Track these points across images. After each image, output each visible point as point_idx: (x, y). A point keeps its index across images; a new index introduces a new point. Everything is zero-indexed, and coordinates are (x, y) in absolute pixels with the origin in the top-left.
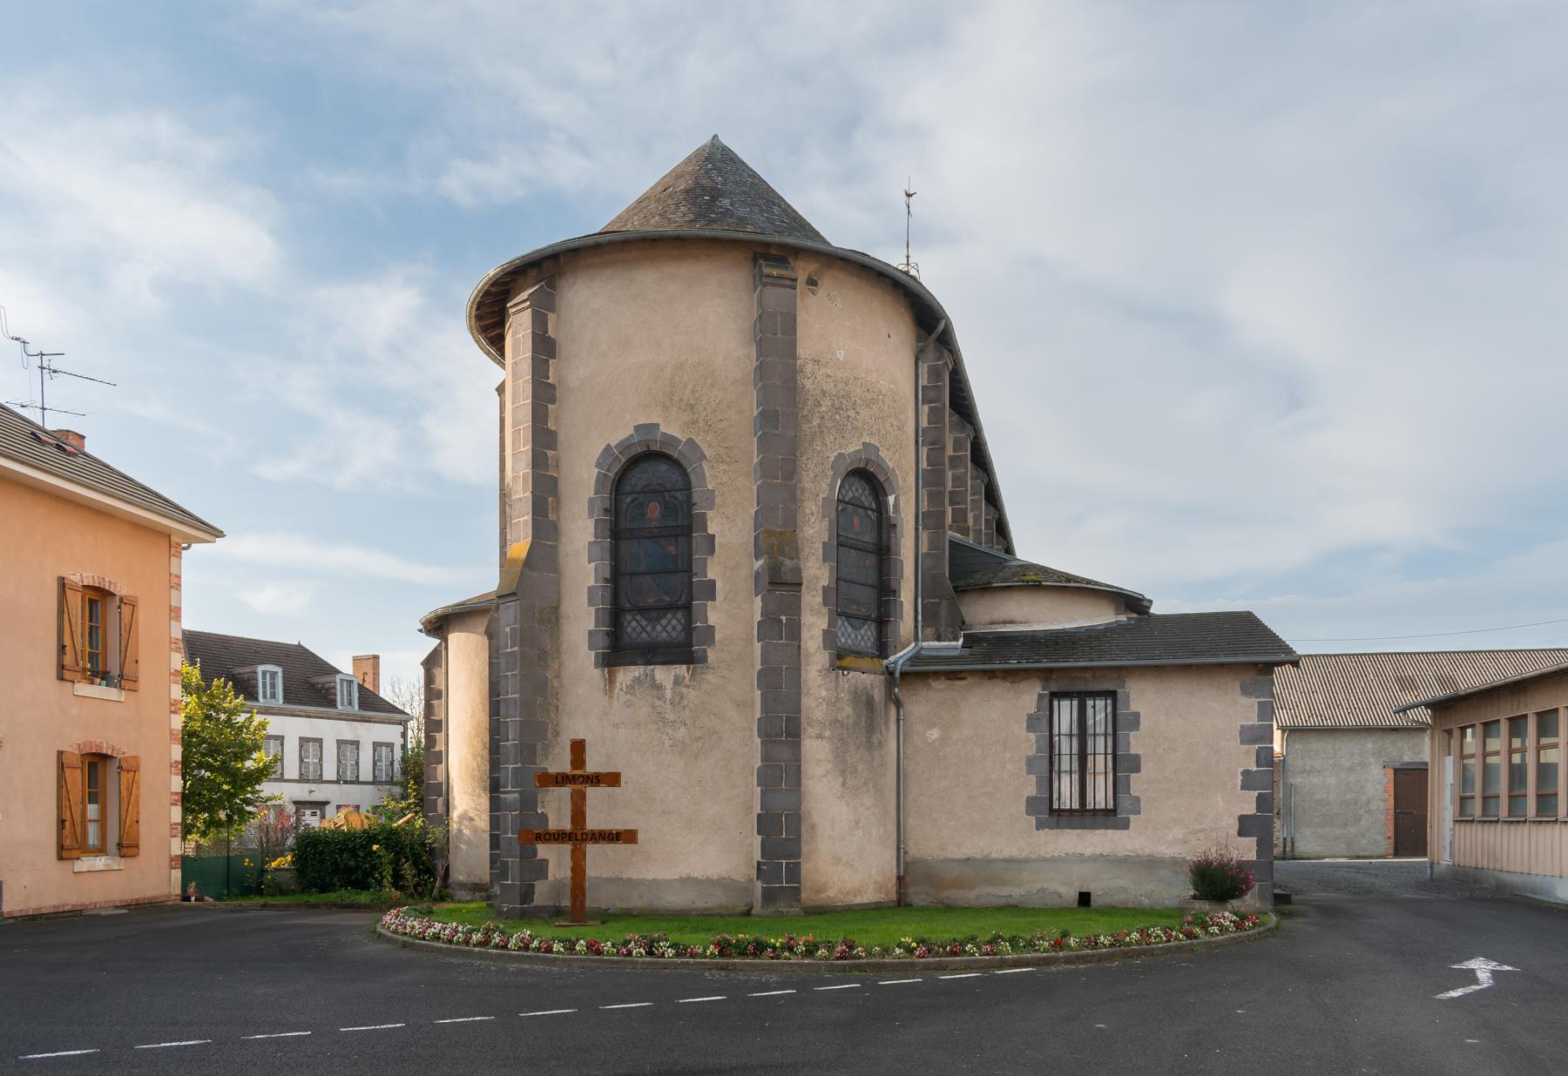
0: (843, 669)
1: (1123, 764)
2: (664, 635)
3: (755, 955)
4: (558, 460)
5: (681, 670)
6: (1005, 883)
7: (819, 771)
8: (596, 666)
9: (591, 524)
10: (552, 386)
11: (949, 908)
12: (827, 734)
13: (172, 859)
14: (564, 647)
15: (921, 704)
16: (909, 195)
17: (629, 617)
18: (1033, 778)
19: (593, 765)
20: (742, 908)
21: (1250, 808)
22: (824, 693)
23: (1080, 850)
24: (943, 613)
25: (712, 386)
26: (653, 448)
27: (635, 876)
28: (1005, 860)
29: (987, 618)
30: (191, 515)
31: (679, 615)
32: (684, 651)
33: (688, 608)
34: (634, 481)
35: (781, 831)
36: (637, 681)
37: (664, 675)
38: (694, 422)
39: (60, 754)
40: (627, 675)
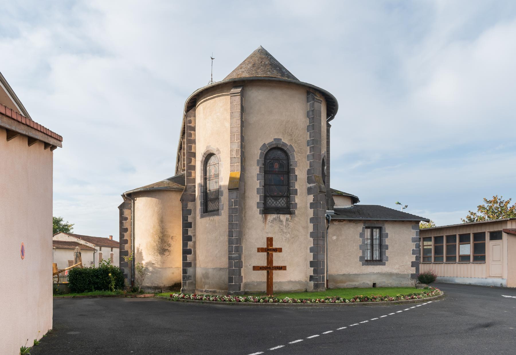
1: (382, 247)
2: (280, 205)
3: (366, 301)
5: (288, 216)
6: (354, 281)
8: (260, 214)
9: (258, 168)
11: (339, 289)
14: (247, 207)
17: (268, 199)
19: (275, 245)
20: (304, 290)
21: (414, 260)
23: (373, 271)
25: (297, 129)
26: (279, 146)
27: (278, 281)
28: (354, 275)
31: (284, 199)
32: (288, 210)
33: (288, 197)
34: (270, 156)
36: (275, 219)
37: (283, 217)
38: (292, 140)
40: (271, 217)
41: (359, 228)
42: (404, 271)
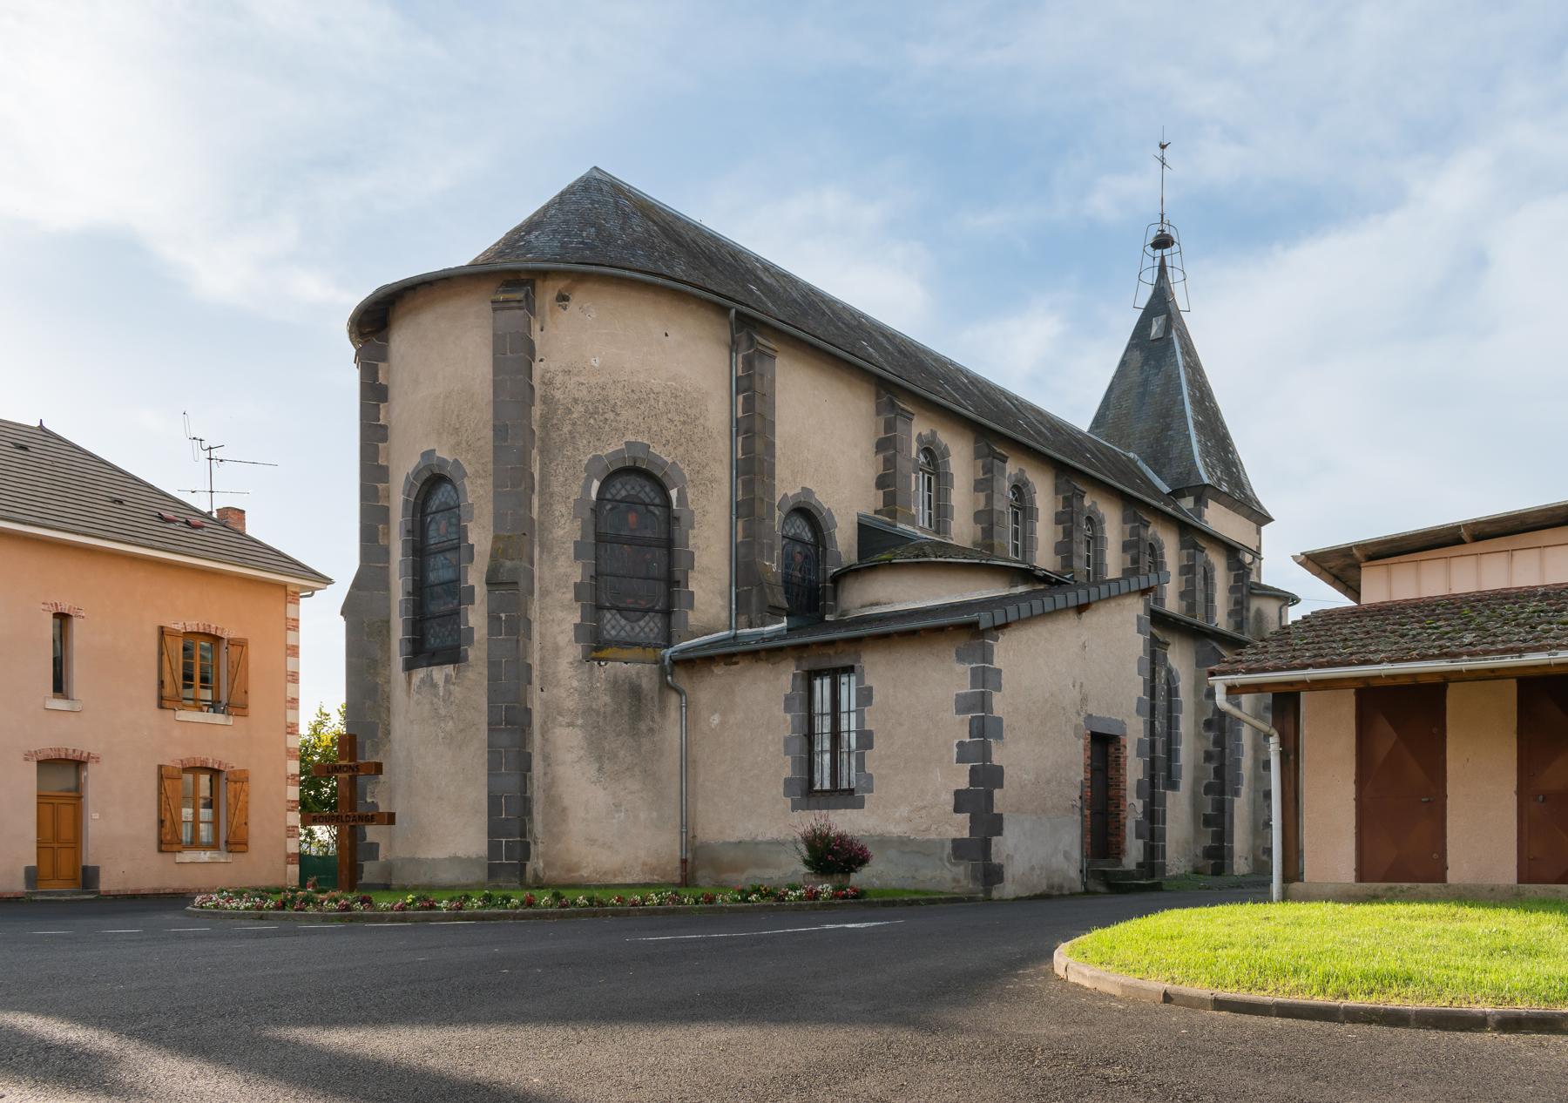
0: (599, 660)
4: (388, 490)
5: (449, 669)
7: (570, 757)
10: (385, 428)
12: (580, 722)
13: (288, 856)
15: (707, 690)
16: (1163, 147)
18: (789, 758)
21: (964, 783)
22: (575, 684)
24: (754, 600)
27: (423, 856)
29: (858, 602)
30: (299, 564)
32: (453, 655)
35: (513, 815)
39: (160, 767)
41: (784, 677)
42: (928, 830)
